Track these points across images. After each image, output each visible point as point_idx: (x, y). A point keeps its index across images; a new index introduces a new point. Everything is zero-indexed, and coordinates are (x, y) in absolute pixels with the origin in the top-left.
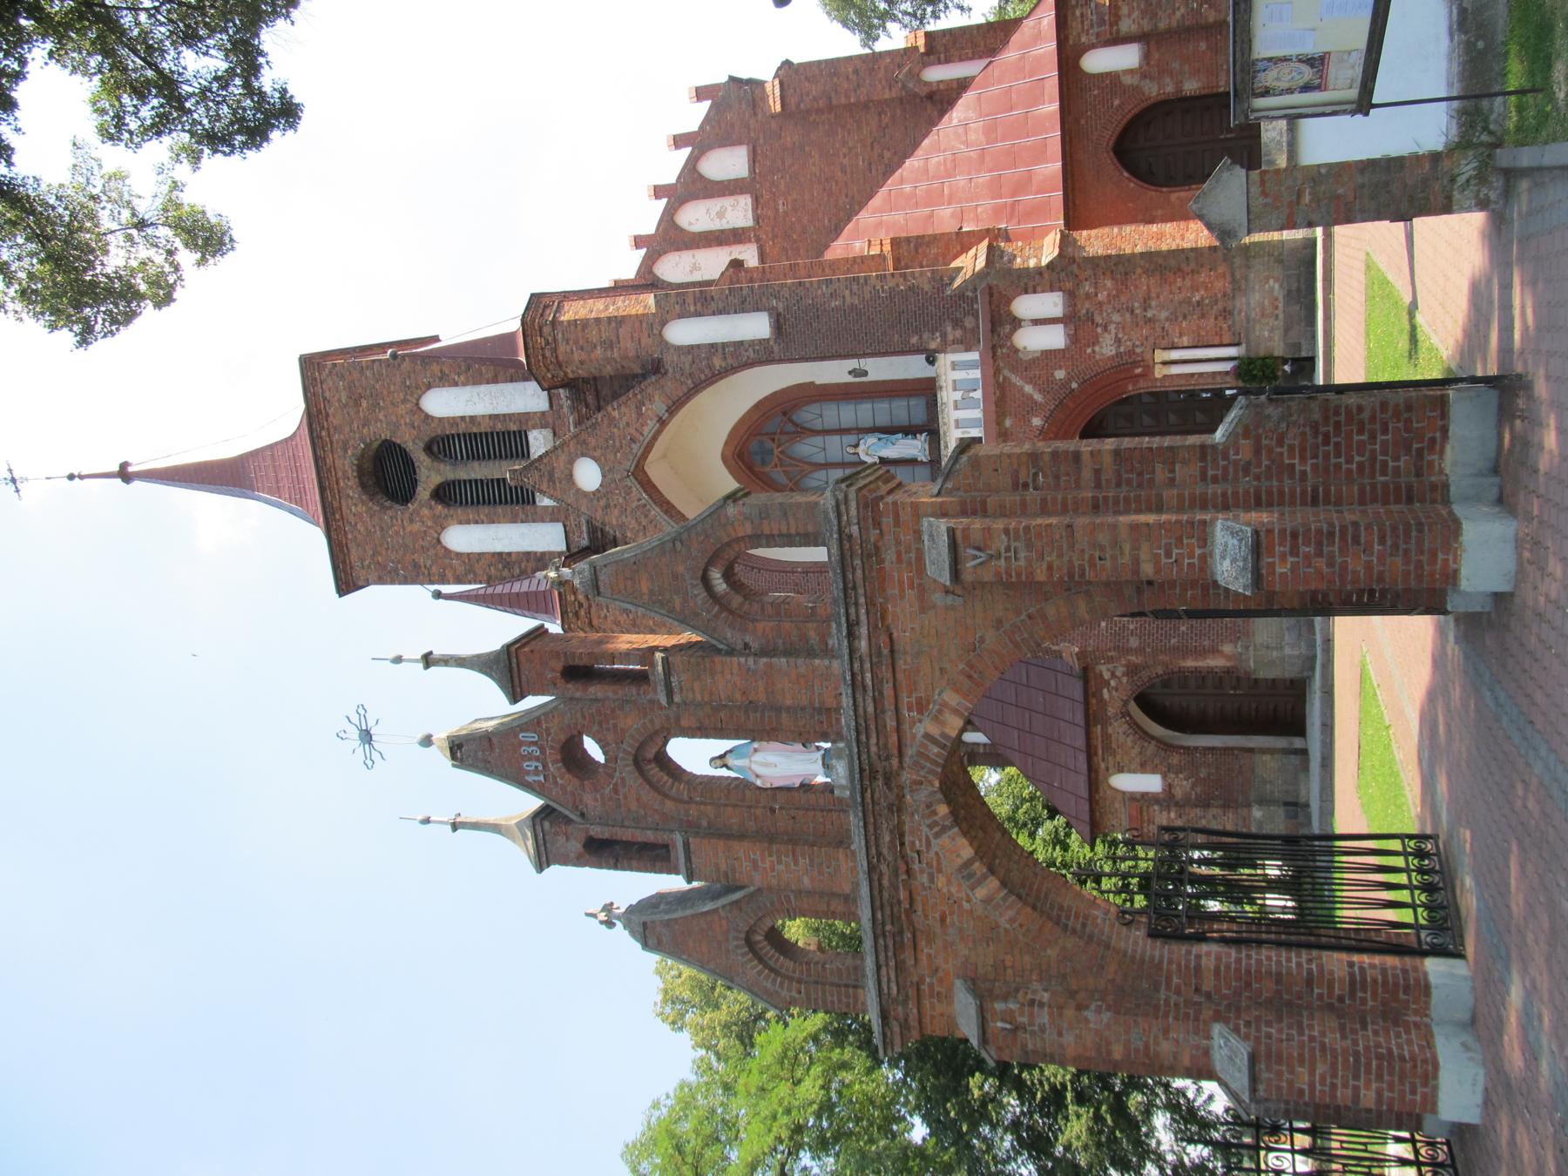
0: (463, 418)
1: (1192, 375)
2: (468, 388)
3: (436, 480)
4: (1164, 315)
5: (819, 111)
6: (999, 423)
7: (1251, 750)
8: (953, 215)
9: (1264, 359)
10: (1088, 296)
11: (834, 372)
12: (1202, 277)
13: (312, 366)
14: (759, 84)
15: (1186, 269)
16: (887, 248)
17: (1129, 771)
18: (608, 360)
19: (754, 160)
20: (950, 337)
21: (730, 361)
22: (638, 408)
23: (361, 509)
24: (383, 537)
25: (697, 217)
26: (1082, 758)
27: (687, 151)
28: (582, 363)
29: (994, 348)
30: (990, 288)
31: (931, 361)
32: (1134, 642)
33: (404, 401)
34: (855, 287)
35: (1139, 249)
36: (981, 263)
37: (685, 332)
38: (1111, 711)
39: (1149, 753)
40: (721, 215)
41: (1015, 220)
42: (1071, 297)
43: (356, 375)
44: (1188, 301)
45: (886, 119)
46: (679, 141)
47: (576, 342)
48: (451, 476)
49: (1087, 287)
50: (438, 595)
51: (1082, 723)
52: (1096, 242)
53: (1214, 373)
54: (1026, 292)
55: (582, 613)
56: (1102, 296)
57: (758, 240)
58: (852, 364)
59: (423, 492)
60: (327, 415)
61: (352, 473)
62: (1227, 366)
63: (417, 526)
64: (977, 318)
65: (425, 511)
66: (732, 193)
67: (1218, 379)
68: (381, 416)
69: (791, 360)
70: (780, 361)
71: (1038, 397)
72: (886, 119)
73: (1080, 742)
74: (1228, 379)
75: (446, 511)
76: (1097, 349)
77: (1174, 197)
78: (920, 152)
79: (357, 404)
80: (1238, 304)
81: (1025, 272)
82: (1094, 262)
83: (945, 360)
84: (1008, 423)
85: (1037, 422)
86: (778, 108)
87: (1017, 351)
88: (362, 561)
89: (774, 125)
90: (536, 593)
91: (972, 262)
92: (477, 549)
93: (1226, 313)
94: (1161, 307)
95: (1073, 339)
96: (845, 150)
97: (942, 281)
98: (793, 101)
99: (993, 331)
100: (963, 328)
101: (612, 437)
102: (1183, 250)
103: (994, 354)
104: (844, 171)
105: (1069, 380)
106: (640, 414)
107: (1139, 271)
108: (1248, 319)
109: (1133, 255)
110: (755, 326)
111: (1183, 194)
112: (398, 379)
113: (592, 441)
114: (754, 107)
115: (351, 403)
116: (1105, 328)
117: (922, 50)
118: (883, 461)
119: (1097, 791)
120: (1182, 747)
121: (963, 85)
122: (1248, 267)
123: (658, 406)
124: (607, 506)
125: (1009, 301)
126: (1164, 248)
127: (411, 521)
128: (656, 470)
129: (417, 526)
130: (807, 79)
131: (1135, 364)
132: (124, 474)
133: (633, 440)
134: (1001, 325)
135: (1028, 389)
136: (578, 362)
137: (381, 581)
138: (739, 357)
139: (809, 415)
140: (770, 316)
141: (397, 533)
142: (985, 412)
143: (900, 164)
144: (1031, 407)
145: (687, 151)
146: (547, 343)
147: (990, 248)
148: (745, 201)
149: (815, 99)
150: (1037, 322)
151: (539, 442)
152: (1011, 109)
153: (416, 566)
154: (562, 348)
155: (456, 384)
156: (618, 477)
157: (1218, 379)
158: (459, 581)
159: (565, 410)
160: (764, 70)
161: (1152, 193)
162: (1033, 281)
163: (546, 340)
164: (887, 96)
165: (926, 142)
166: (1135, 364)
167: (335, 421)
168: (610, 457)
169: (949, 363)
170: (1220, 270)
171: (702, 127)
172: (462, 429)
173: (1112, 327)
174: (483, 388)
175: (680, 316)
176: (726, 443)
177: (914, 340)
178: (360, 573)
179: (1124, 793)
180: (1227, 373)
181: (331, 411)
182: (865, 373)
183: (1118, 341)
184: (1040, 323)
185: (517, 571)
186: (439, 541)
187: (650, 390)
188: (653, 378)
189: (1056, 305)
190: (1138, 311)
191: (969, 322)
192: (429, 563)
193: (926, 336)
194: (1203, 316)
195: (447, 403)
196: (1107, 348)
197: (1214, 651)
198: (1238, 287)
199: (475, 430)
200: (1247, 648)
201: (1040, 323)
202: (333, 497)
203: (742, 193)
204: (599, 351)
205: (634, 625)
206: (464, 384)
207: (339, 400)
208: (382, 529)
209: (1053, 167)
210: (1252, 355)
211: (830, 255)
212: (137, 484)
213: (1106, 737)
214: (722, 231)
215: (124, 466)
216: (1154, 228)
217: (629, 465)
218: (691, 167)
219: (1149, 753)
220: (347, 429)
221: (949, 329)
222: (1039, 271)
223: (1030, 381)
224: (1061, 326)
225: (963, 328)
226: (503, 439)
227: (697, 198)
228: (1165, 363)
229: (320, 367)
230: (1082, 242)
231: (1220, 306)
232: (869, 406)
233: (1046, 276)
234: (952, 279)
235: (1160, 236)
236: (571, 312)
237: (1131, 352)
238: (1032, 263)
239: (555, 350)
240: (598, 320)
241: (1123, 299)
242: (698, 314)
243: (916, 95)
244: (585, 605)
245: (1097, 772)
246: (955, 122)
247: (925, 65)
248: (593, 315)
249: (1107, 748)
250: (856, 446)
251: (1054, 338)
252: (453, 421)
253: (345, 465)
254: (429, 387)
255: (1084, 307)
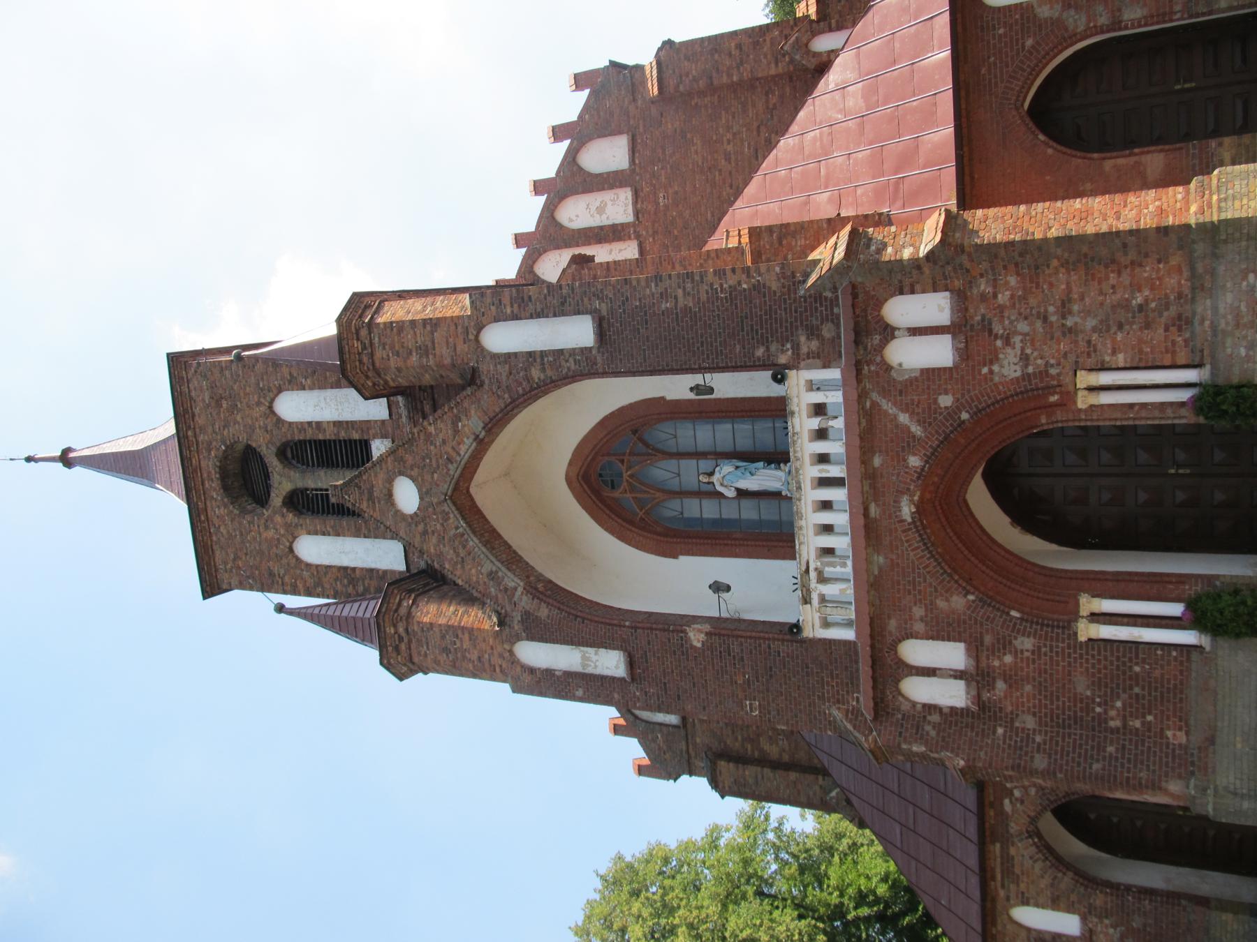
0: (310, 423)
1: (1131, 406)
2: (316, 393)
3: (287, 487)
4: (1091, 323)
5: (702, 94)
6: (865, 462)
7: (1203, 902)
8: (830, 200)
9: (1239, 387)
10: (983, 297)
11: (678, 387)
12: (1147, 272)
13: (179, 364)
14: (639, 68)
15: (1124, 260)
16: (745, 239)
17: (1037, 905)
18: (425, 368)
19: (633, 150)
20: (804, 350)
21: (549, 373)
22: (455, 424)
23: (222, 511)
24: (243, 542)
25: (578, 213)
26: (974, 881)
27: (567, 143)
28: (399, 370)
29: (858, 366)
30: (854, 286)
31: (779, 378)
32: (1040, 762)
33: (259, 404)
34: (689, 286)
35: (1054, 233)
36: (840, 254)
37: (504, 338)
38: (1014, 828)
39: (1063, 886)
40: (601, 210)
41: (899, 203)
42: (961, 300)
43: (217, 375)
44: (1125, 305)
45: (774, 100)
46: (558, 133)
47: (392, 348)
48: (300, 485)
49: (984, 286)
50: (280, 608)
51: (975, 838)
52: (994, 224)
53: (1162, 404)
54: (901, 293)
55: (403, 647)
56: (1003, 298)
57: (638, 237)
58: (697, 379)
59: (277, 500)
60: (193, 416)
61: (216, 476)
62: (1184, 396)
63: (271, 533)
64: (838, 326)
65: (278, 519)
66: (611, 187)
67: (1169, 412)
68: (239, 418)
69: (617, 374)
70: (604, 374)
71: (916, 430)
72: (774, 100)
73: (973, 862)
74: (1183, 412)
75: (296, 520)
76: (996, 368)
77: (1108, 165)
78: (794, 128)
79: (219, 405)
80: (1199, 310)
81: (898, 266)
82: (992, 250)
83: (798, 379)
84: (877, 461)
85: (914, 461)
86: (656, 91)
87: (889, 368)
88: (225, 563)
89: (654, 111)
90: (362, 619)
91: (830, 252)
92: (326, 561)
93: (1182, 322)
94: (1087, 313)
95: (964, 354)
96: (729, 136)
97: (793, 279)
98: (671, 83)
99: (857, 342)
100: (820, 337)
101: (428, 456)
102: (1118, 233)
103: (859, 372)
104: (728, 160)
105: (957, 409)
106: (456, 432)
107: (1055, 263)
108: (1214, 327)
109: (1045, 240)
110: (576, 332)
111: (1121, 161)
112: (253, 380)
113: (409, 459)
114: (633, 93)
115: (213, 404)
116: (1007, 341)
117: (814, 17)
118: (742, 493)
119: (994, 924)
120: (1108, 884)
121: (833, 54)
122: (1215, 256)
123: (473, 423)
124: (425, 533)
125: (880, 304)
126: (1090, 229)
127: (267, 528)
128: (488, 492)
129: (271, 533)
130: (687, 58)
131: (1050, 390)
132: (66, 459)
133: (450, 460)
134: (869, 333)
135: (904, 418)
136: (395, 367)
137: (242, 586)
138: (558, 371)
139: (664, 434)
140: (593, 319)
141: (255, 539)
142: (848, 445)
143: (770, 145)
144: (908, 443)
145: (567, 143)
146: (364, 348)
147: (853, 233)
148: (625, 195)
149: (695, 80)
150: (915, 331)
151: (379, 448)
152: (895, 63)
153: (271, 574)
154: (379, 353)
155: (303, 388)
156: (435, 500)
157: (1169, 412)
158: (309, 593)
159: (404, 419)
160: (642, 54)
161: (1077, 162)
162: (908, 277)
163: (364, 342)
164: (773, 72)
165: (801, 114)
166: (1050, 390)
167: (200, 421)
168: (428, 477)
169: (802, 383)
170: (1174, 261)
171: (580, 117)
172: (309, 435)
173: (1017, 340)
174: (330, 393)
175: (497, 320)
176: (570, 464)
177: (760, 352)
178: (224, 577)
179: (1029, 930)
180: (1182, 404)
181: (197, 411)
182: (711, 390)
183: (1025, 359)
184: (920, 332)
185: (361, 589)
186: (291, 550)
187: (466, 404)
188: (469, 391)
189: (941, 310)
190: (1053, 319)
191: (827, 331)
192: (282, 572)
193: (773, 348)
194: (1147, 326)
195: (299, 407)
196: (1009, 368)
197: (1155, 786)
198: (1199, 286)
199: (321, 437)
200: (1205, 790)
201: (920, 332)
202: (199, 498)
203: (621, 186)
204: (414, 358)
205: (454, 666)
206: (311, 388)
207: (203, 400)
208: (241, 534)
209: (943, 134)
210: (1221, 381)
211: (707, 248)
212: (78, 470)
213: (1007, 859)
214: (601, 228)
215: (66, 451)
216: (1077, 204)
217: (446, 487)
218: (570, 160)
219: (1063, 886)
220: (210, 430)
221: (803, 339)
222: (916, 264)
223: (905, 409)
224: (947, 339)
225: (820, 337)
226: (343, 449)
227: (577, 193)
228: (1092, 389)
229: (187, 366)
230: (975, 225)
231: (1173, 311)
232: (729, 426)
233: (926, 270)
234: (807, 275)
235: (1085, 215)
236: (392, 313)
237: (1044, 374)
238: (907, 254)
239: (372, 355)
240: (413, 322)
241: (1033, 301)
242: (515, 317)
243: (806, 70)
244: (406, 640)
245: (994, 900)
246: (832, 87)
247: (815, 34)
248: (410, 317)
249: (1008, 871)
250: (711, 474)
251: (938, 353)
252: (303, 426)
253: (209, 465)
254: (280, 391)
255: (978, 313)
